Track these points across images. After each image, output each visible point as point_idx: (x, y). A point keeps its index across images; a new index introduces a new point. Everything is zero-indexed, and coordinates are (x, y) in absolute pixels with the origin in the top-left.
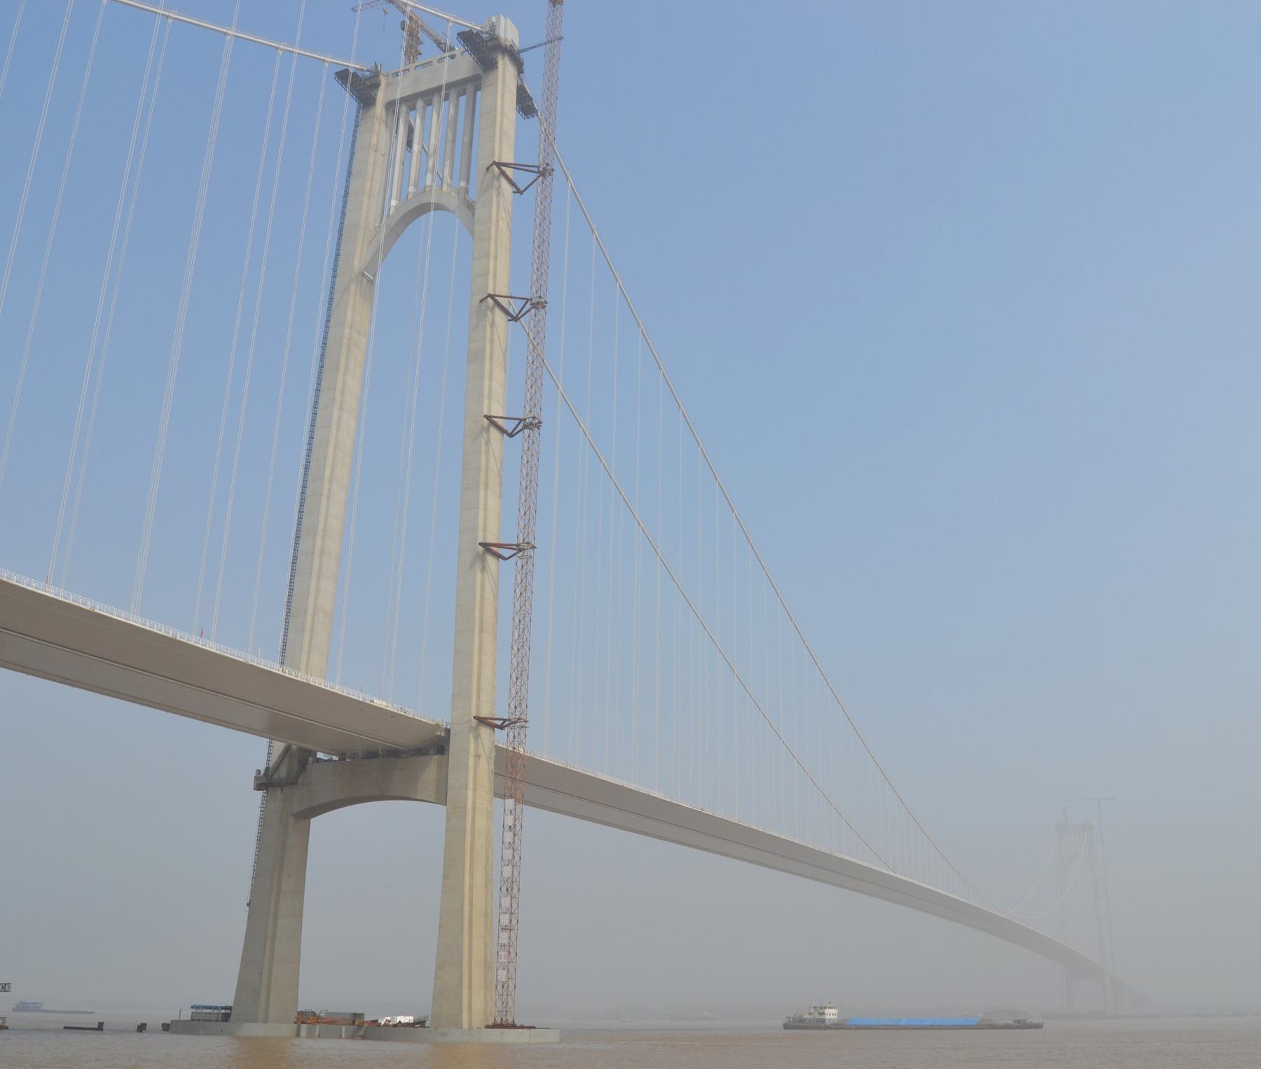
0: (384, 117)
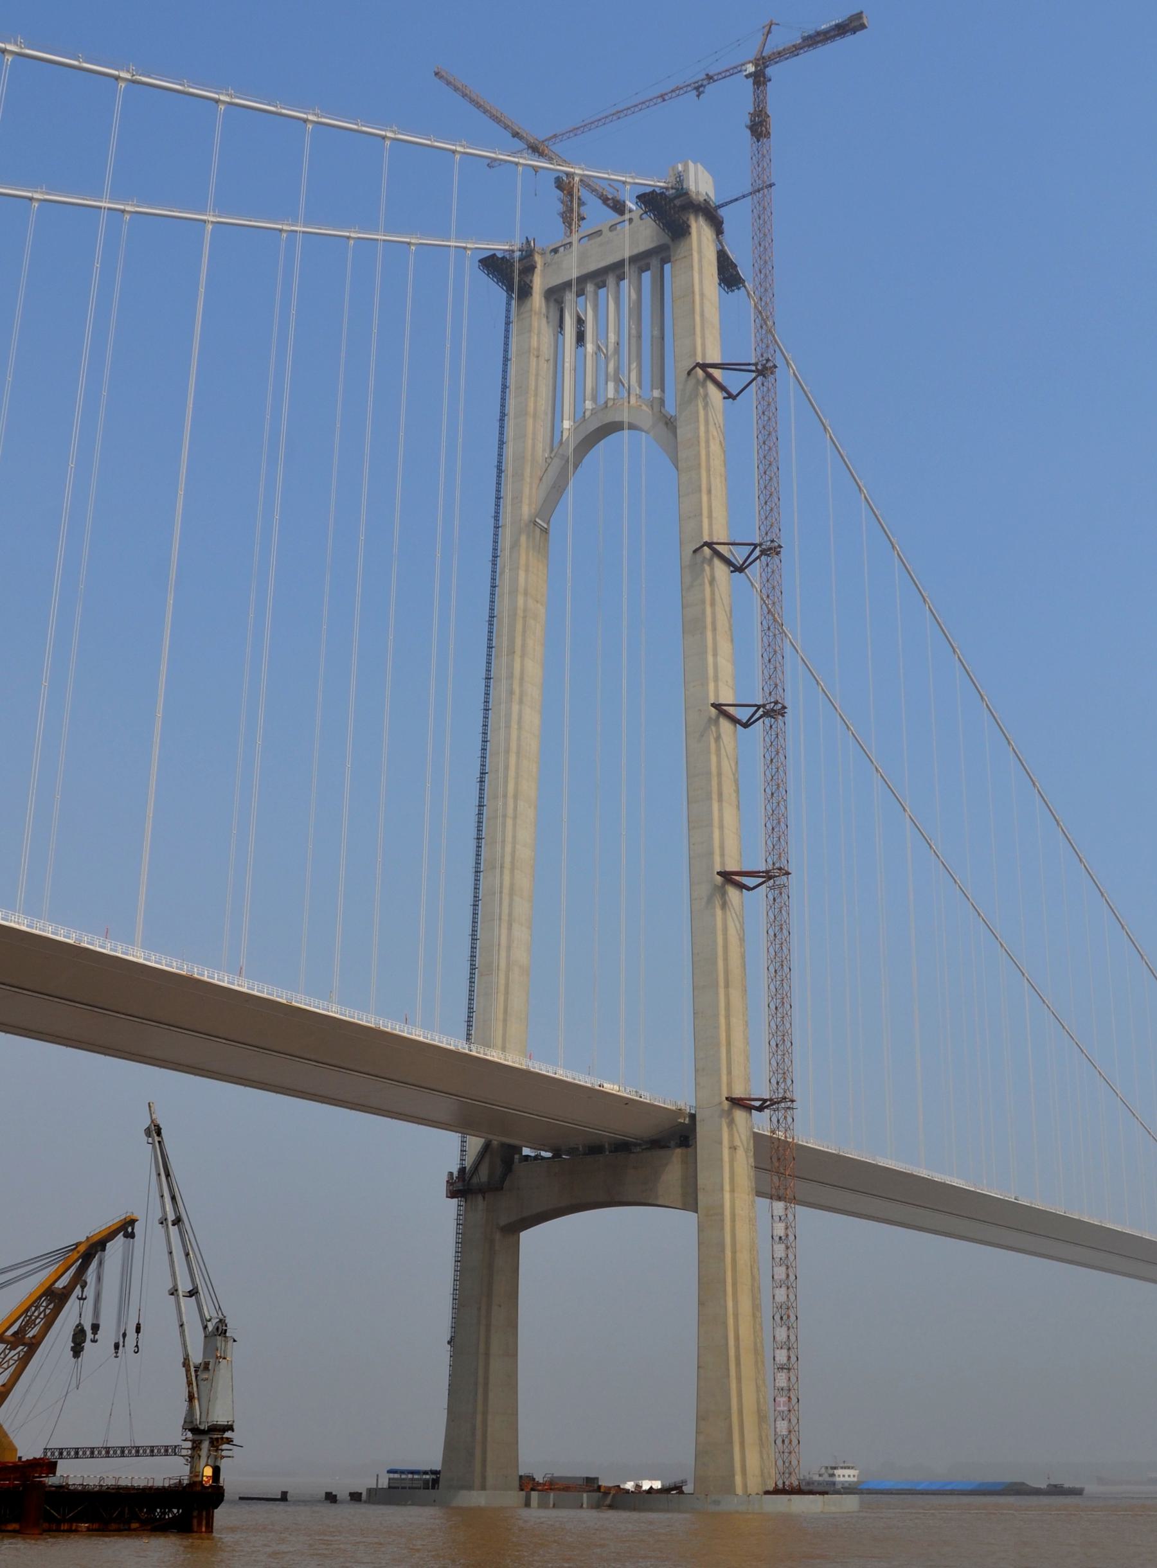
0: (544, 310)
